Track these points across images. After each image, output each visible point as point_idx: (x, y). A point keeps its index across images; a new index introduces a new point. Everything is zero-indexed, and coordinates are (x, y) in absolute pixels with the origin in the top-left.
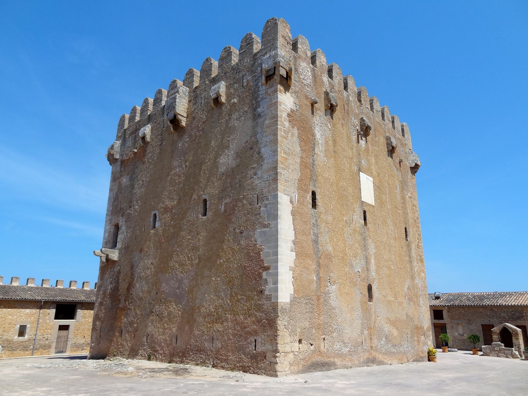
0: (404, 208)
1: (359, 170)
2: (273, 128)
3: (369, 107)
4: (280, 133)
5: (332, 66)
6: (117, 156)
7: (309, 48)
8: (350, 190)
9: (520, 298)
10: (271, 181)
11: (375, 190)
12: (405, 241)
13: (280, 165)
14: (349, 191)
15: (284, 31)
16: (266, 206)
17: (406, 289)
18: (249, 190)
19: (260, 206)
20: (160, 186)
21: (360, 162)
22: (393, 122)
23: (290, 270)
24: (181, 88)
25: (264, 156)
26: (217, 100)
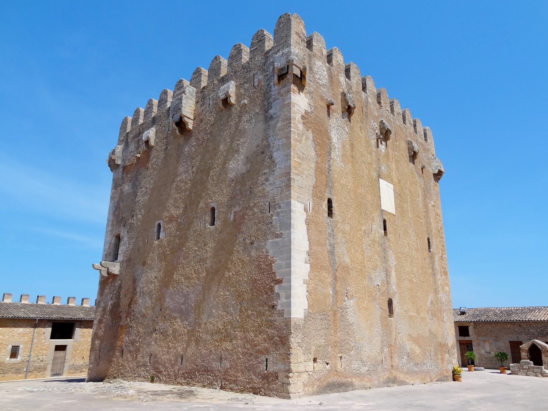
0: (427, 217)
1: (379, 176)
2: (286, 131)
3: (389, 110)
4: (294, 136)
5: (350, 66)
6: (119, 162)
7: (324, 46)
8: (369, 197)
10: (284, 188)
11: (395, 198)
12: (428, 252)
13: (293, 171)
14: (368, 199)
15: (298, 27)
16: (278, 214)
17: (429, 304)
18: (260, 197)
19: (272, 215)
20: (164, 193)
21: (380, 168)
22: (415, 126)
23: (304, 283)
24: (187, 88)
25: (276, 161)
26: (226, 101)
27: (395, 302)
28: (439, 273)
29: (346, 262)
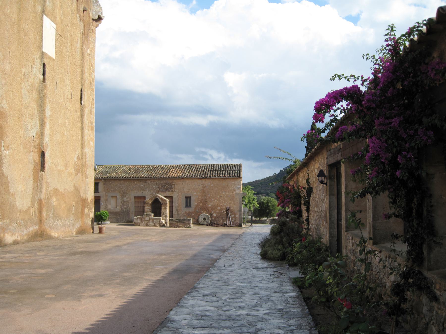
0: (82, 67)
1: (43, 12)
8: (32, 35)
9: (171, 171)
11: (57, 40)
12: (79, 104)
17: (76, 159)
27: (47, 155)
28: (87, 128)
29: (5, 108)
